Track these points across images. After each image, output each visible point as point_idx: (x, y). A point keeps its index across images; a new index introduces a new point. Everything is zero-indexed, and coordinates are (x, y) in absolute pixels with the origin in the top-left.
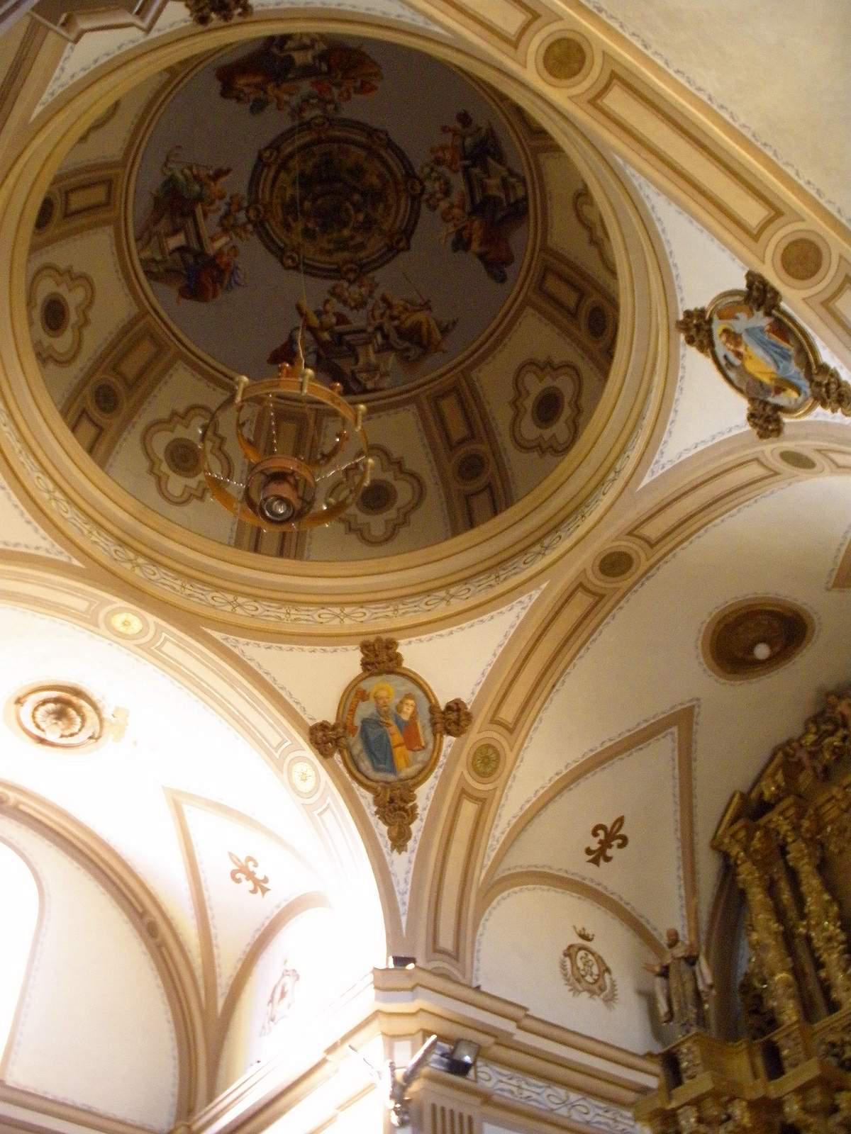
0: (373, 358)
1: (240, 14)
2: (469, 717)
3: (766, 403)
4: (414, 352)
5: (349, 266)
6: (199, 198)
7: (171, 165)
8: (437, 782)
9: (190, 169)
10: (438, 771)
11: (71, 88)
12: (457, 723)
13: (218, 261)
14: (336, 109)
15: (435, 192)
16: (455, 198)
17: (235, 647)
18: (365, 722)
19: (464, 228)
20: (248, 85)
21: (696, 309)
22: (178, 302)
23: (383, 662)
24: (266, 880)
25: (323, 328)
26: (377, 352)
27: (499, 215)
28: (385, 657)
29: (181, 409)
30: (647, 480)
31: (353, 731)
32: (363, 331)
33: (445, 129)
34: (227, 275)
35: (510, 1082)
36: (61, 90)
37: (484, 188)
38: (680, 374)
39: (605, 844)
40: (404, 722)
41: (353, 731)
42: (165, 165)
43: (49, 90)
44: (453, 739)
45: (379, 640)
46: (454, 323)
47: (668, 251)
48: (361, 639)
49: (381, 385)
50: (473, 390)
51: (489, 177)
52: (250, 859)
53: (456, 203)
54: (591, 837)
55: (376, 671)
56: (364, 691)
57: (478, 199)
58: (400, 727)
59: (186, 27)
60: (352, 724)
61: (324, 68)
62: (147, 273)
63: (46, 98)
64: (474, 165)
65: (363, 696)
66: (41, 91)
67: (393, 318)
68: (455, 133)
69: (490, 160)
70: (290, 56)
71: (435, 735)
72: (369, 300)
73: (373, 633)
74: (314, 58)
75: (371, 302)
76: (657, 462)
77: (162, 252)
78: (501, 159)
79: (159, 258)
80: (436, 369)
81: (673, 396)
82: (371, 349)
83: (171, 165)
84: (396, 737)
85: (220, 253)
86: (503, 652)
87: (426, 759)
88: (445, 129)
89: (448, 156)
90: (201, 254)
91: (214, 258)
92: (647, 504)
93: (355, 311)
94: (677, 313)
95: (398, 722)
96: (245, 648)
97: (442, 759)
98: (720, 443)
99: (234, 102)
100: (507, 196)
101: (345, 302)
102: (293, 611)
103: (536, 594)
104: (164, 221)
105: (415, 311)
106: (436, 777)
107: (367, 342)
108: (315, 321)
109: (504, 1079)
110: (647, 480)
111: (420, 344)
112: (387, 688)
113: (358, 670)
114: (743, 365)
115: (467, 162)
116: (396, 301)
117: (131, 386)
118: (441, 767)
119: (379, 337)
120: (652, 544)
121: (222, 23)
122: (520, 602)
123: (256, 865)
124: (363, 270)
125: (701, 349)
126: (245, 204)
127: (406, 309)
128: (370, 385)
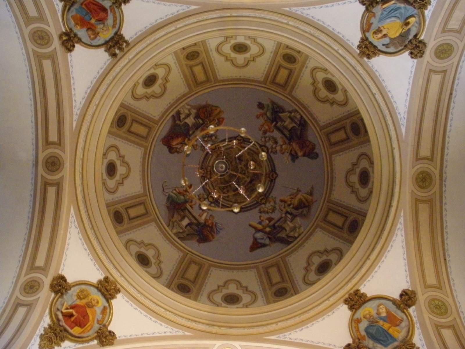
0: (291, 225)
1: (126, 46)
2: (413, 293)
3: (410, 41)
4: (305, 211)
5: (260, 198)
6: (186, 202)
7: (166, 191)
8: (420, 331)
9: (175, 190)
10: (417, 326)
11: (82, 109)
12: (410, 298)
13: (207, 224)
14: (216, 138)
15: (272, 146)
16: (280, 142)
17: (285, 338)
18: (366, 330)
19: (291, 151)
20: (177, 144)
21: (360, 42)
22: (198, 245)
23: (358, 300)
25: (265, 228)
26: (291, 222)
27: (299, 133)
28: (357, 298)
29: (221, 283)
30: (403, 130)
31: (363, 338)
32: (281, 218)
33: (258, 117)
34: (214, 227)
37: (286, 128)
38: (378, 75)
40: (384, 317)
41: (363, 338)
42: (163, 191)
43: (75, 113)
44: (413, 307)
45: (350, 294)
46: (312, 188)
48: (342, 300)
49: (301, 232)
50: (338, 205)
51: (285, 122)
53: (282, 144)
55: (357, 306)
56: (358, 318)
57: (287, 134)
58: (385, 321)
60: (361, 335)
61: (201, 122)
62: (179, 238)
63: (75, 117)
64: (277, 123)
65: (359, 321)
66: (71, 114)
67: (289, 205)
68: (262, 115)
69: (281, 115)
70: (186, 123)
71: (404, 312)
72: (276, 205)
73: (347, 293)
74: (194, 119)
75: (277, 206)
77: (182, 228)
78: (283, 111)
79: (181, 231)
80: (317, 210)
81: (383, 86)
82: (288, 222)
83: (166, 191)
84: (386, 326)
85: (206, 220)
86: (407, 255)
87: (407, 323)
88: (258, 117)
89: (267, 127)
90: (198, 224)
91: (205, 223)
92: (411, 140)
93: (273, 213)
94: (356, 52)
95: (384, 319)
96: (290, 336)
97: (415, 319)
99: (176, 154)
100: (296, 123)
101: (267, 212)
103: (402, 220)
104: (175, 216)
105: (296, 196)
106: (418, 329)
107: (285, 221)
108: (260, 227)
110: (403, 130)
111: (305, 206)
112: (106, 35)
113: (349, 313)
114: (391, 39)
115: (274, 123)
116: (287, 198)
117: (194, 282)
118: (417, 323)
119: (289, 216)
120: (431, 159)
121: (122, 53)
122: (398, 229)
124: (267, 196)
125: (375, 54)
126: (205, 196)
127: (292, 198)
128: (296, 235)
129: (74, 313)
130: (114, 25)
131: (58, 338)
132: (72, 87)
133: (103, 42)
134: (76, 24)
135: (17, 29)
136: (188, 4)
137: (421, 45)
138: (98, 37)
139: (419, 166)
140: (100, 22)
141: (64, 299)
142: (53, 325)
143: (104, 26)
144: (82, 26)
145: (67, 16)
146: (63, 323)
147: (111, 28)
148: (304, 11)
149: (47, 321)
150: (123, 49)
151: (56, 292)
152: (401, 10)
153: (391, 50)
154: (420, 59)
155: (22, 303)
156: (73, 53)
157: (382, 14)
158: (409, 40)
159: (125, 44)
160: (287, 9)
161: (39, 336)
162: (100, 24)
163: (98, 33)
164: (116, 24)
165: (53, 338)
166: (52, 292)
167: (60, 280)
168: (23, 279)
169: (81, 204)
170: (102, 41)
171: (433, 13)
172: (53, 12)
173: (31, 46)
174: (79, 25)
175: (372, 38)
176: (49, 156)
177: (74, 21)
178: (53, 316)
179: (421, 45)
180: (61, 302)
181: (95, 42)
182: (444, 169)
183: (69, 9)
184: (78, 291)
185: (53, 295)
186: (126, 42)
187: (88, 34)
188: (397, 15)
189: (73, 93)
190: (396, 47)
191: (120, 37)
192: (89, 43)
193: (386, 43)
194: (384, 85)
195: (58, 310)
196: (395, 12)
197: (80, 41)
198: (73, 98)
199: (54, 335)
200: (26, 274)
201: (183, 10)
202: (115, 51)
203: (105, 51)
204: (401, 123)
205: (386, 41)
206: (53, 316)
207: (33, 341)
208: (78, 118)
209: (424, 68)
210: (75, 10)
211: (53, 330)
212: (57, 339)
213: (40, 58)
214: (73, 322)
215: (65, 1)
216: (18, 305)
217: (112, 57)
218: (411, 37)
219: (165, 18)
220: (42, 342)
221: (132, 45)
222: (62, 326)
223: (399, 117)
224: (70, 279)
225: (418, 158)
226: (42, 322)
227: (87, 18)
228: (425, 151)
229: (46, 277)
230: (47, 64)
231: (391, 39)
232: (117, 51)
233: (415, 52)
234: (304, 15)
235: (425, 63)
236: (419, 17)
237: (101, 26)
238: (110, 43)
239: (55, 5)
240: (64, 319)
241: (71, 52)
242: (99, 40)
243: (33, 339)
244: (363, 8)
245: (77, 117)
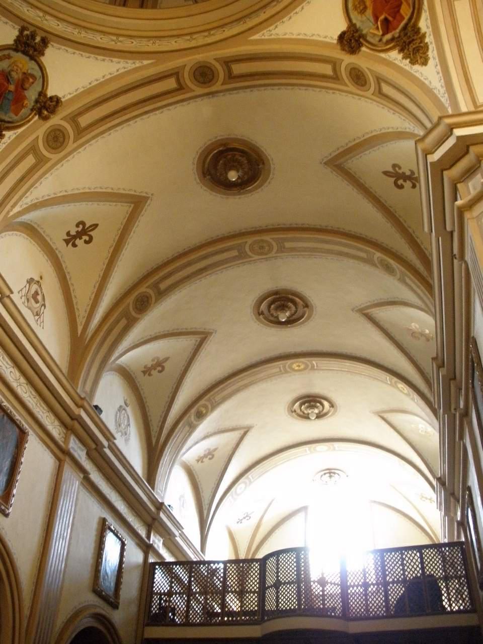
1: (28, 30)
11: (125, 58)
35: (34, 399)
36: (129, 61)
39: (79, 235)
43: (133, 66)
54: (75, 227)
59: (55, 42)
63: (138, 64)
66: (136, 70)
109: (32, 397)
112: (23, 63)
121: (38, 31)
129: (382, 17)
130: (6, 58)
131: (415, 37)
132: (102, 80)
133: (33, 62)
134: (23, 107)
135: (58, 166)
138: (29, 72)
140: (9, 78)
141: (367, 32)
142: (399, 46)
143: (13, 71)
144: (24, 98)
145: (18, 122)
146: (396, 33)
147: (12, 60)
149: (395, 56)
150: (31, 32)
151: (360, 45)
155: (377, 89)
156: (60, 95)
159: (26, 33)
161: (412, 66)
162: (11, 77)
163: (24, 73)
164: (4, 55)
165: (414, 46)
166: (360, 51)
167: (344, 41)
168: (352, 88)
169: (250, 23)
170: (33, 64)
172: (19, 139)
173: (71, 146)
174: (23, 103)
176: (195, 82)
177: (21, 110)
178: (388, 47)
180: (372, 38)
181: (37, 73)
183: (9, 122)
184: (356, 13)
185: (364, 49)
186: (21, 31)
187: (30, 86)
189: (109, 76)
191: (18, 42)
192: (41, 79)
195: (380, 40)
197: (42, 94)
198: (115, 74)
199: (412, 45)
200: (346, 85)
202: (40, 41)
203: (43, 54)
206: (388, 47)
207: (417, 75)
208: (139, 59)
210: (7, 115)
211: (405, 46)
212: (416, 39)
213: (80, 132)
214: (394, 18)
215: (2, 132)
216: (380, 93)
217: (48, 42)
220: (419, 62)
221: (22, 23)
222: (400, 32)
224: (342, 26)
226: (396, 62)
227: (10, 97)
229: (343, 60)
230: (84, 121)
232: (38, 39)
237: (14, 74)
238: (31, 52)
239: (11, 140)
240: (391, 32)
241: (60, 98)
242: (33, 69)
243: (415, 74)
245: (138, 61)
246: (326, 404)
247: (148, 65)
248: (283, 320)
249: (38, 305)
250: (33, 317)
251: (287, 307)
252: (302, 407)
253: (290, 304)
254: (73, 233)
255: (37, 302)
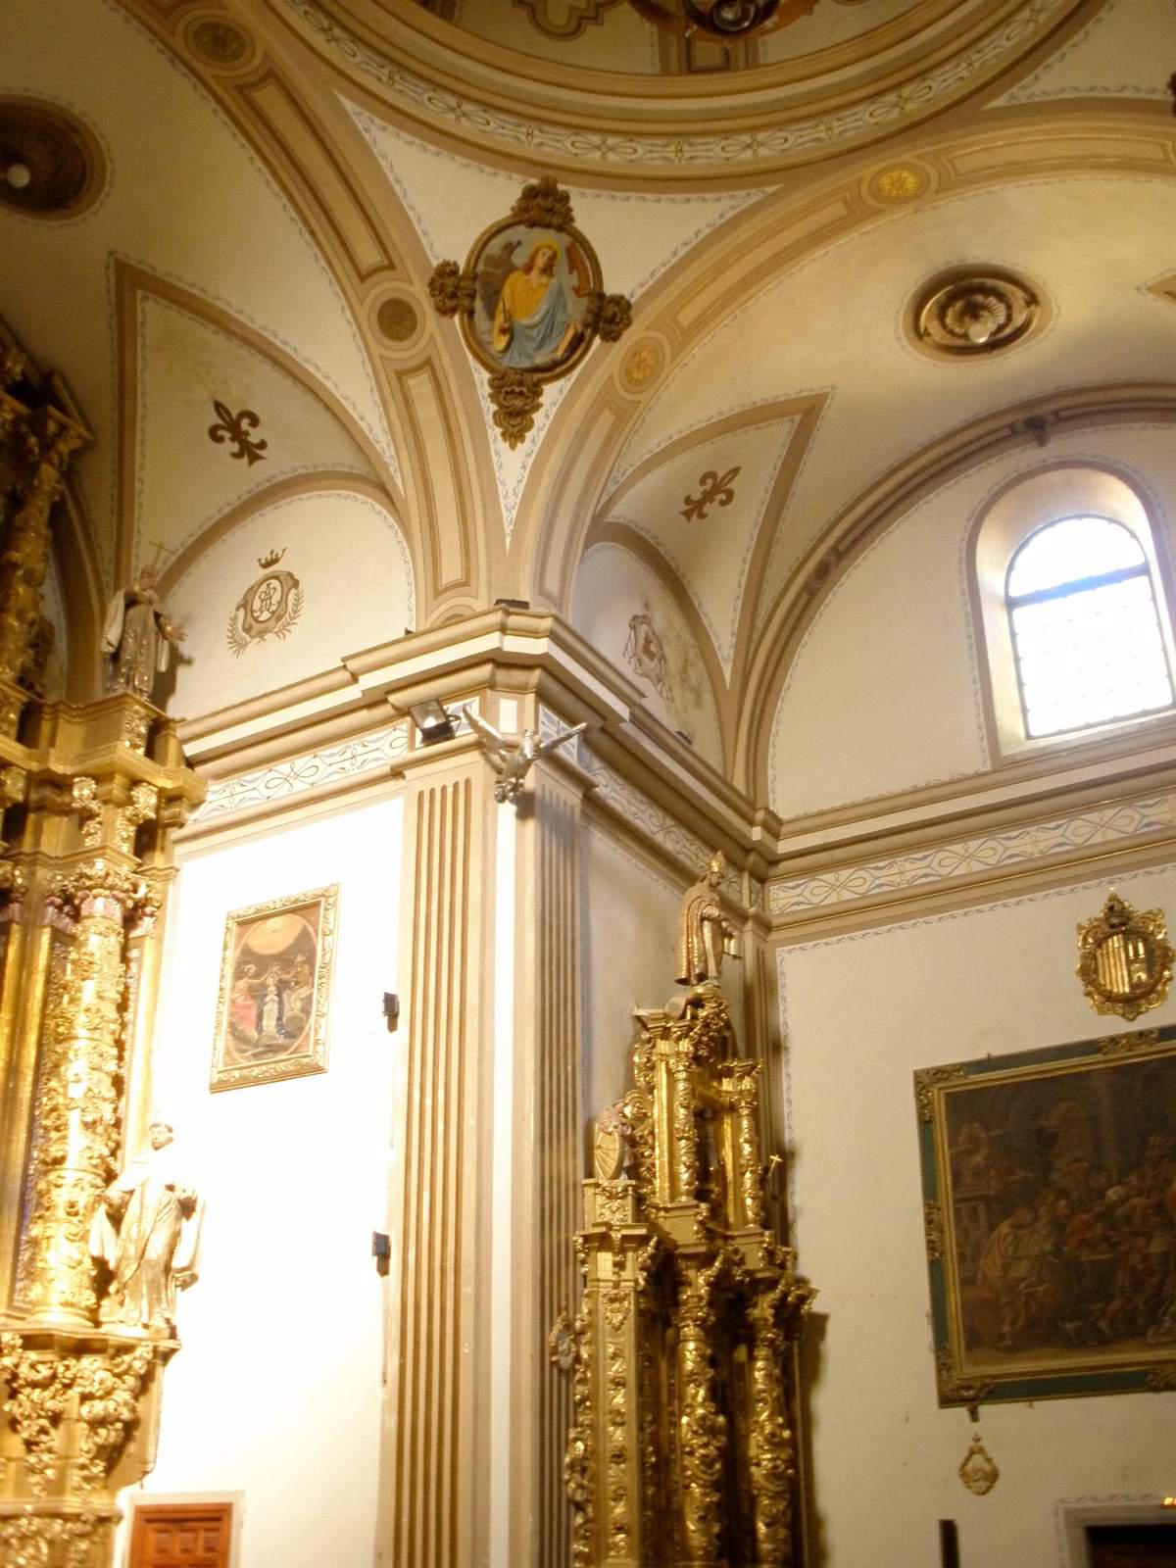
3: (472, 296)
21: (570, 210)
24: (702, 516)
30: (348, 104)
43: (752, 200)
46: (519, 243)
47: (648, 196)
52: (730, 495)
76: (372, 121)
94: (565, 182)
98: (407, 218)
102: (686, 148)
110: (348, 104)
123: (723, 503)
136: (1014, 107)
137: (450, 304)
139: (256, 61)
148: (733, 202)
152: (534, 345)
153: (495, 246)
154: (429, 275)
157: (565, 306)
158: (478, 295)
160: (770, 189)
171: (473, 384)
175: (548, 240)
179: (450, 304)
182: (194, 80)
188: (534, 333)
190: (491, 261)
193: (517, 251)
194: (458, 158)
196: (542, 334)
201: (1024, 87)
204: (367, 114)
205: (519, 258)
209: (409, 264)
218: (478, 304)
219: (1065, 48)
223: (378, 121)
225: (272, 75)
228: (269, 98)
231: (513, 268)
233: (450, 281)
234: (725, 194)
235: (414, 277)
236: (491, 356)
244: (610, 288)
246: (1018, 296)
247: (773, 194)
248: (982, 340)
249: (656, 661)
250: (653, 688)
251: (985, 307)
252: (948, 320)
253: (992, 300)
254: (235, 447)
255: (651, 655)
